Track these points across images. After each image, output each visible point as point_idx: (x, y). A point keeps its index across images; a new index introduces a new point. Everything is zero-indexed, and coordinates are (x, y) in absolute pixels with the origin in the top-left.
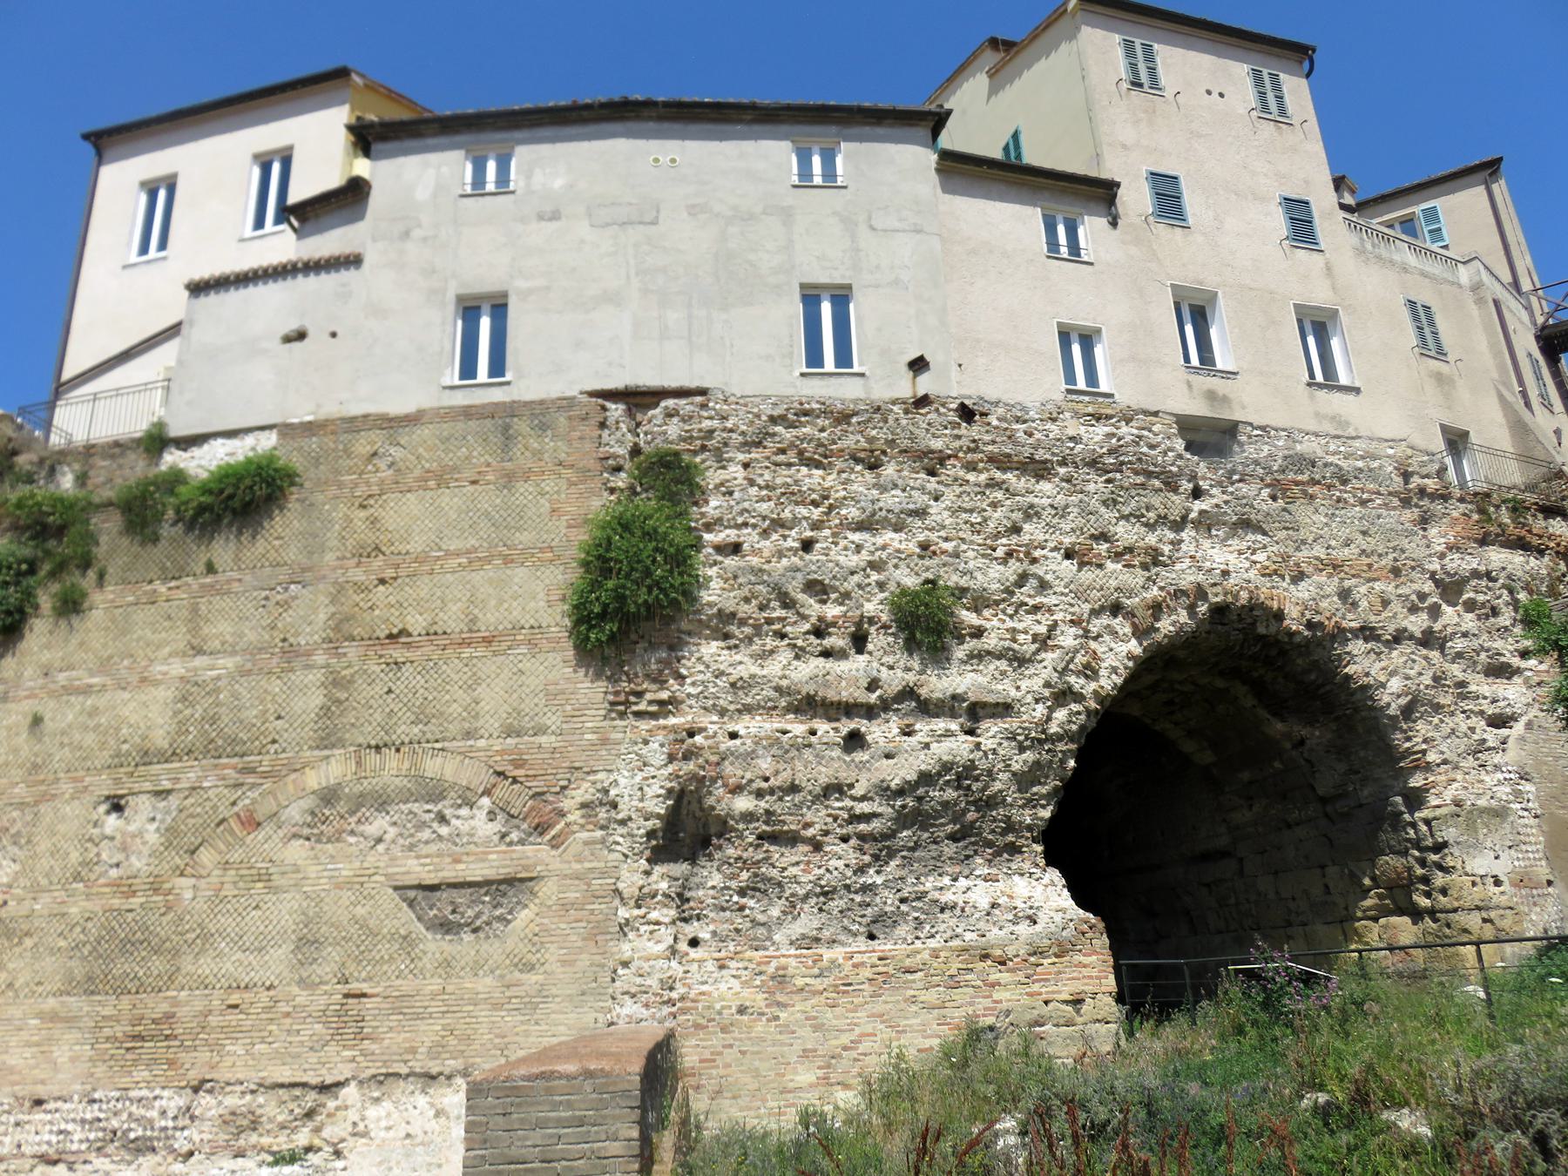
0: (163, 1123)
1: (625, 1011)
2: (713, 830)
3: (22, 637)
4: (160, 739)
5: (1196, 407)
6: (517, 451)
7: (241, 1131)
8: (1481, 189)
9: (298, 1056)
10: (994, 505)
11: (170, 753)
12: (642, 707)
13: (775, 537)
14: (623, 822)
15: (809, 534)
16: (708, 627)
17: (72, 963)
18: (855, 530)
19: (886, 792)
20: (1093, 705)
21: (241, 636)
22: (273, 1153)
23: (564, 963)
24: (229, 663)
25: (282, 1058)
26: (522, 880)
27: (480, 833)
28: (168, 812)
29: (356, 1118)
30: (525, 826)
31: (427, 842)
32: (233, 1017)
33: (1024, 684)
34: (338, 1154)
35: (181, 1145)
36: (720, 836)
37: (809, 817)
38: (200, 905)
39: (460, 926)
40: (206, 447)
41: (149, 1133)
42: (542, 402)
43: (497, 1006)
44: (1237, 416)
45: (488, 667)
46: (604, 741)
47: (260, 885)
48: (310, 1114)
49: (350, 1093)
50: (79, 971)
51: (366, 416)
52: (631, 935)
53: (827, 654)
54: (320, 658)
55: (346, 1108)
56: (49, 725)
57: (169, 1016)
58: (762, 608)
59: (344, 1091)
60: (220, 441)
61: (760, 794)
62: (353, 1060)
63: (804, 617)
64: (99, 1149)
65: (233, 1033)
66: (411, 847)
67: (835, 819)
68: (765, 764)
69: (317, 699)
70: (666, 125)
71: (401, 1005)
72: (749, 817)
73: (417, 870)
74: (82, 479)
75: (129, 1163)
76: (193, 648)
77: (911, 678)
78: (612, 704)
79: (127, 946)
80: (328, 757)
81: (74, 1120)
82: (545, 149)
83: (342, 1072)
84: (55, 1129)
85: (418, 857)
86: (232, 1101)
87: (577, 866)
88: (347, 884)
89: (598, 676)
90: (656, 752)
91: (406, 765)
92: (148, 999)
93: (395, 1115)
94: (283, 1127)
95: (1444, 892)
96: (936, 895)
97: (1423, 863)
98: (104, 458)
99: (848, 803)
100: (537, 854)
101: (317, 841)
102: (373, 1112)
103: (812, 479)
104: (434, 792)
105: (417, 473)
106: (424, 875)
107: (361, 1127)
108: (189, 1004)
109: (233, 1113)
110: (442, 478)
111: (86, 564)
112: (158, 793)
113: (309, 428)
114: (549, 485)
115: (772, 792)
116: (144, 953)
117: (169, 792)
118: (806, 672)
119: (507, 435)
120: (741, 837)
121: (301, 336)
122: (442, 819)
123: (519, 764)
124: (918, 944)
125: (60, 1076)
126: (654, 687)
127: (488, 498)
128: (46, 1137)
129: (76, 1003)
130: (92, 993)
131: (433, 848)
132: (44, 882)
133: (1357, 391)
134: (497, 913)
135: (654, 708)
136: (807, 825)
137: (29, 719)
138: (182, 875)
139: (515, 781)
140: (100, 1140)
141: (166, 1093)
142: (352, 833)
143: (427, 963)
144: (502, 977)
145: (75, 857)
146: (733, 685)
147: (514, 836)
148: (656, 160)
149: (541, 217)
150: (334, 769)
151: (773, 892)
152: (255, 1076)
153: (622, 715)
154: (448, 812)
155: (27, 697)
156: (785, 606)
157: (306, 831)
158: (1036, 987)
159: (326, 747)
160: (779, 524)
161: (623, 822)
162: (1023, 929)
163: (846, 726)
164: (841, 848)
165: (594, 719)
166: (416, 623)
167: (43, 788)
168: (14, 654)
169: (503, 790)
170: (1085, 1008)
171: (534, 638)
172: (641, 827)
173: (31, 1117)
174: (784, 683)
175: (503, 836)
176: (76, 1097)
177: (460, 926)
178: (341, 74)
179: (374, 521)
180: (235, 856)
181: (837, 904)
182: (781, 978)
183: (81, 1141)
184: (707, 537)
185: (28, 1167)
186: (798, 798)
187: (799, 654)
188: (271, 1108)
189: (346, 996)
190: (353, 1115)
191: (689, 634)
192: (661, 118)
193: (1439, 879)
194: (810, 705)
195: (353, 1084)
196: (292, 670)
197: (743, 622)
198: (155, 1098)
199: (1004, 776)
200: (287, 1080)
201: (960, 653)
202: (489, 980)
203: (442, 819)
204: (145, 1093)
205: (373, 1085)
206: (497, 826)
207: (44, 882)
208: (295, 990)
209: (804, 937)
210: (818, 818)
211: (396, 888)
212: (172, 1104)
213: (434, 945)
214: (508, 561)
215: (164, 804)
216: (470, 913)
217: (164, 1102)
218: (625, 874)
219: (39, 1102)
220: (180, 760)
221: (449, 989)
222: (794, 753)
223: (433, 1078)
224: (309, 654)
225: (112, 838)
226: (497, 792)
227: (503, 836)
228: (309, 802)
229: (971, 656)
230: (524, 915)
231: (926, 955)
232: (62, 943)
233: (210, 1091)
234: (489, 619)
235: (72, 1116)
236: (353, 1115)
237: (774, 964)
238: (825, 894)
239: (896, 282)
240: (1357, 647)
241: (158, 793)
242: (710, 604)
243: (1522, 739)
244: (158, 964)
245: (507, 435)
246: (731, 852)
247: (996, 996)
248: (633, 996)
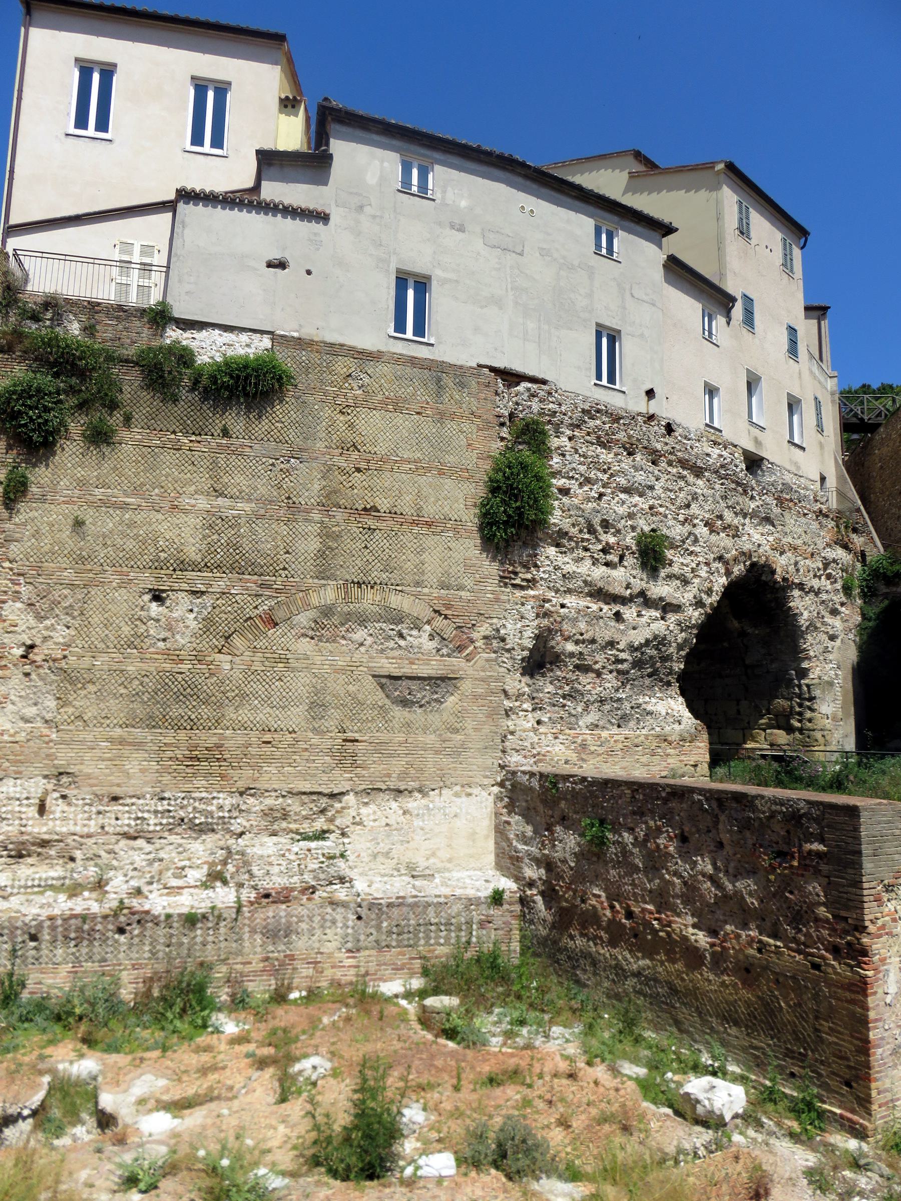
0: (221, 814)
1: (514, 759)
2: (547, 660)
3: (54, 454)
4: (192, 552)
5: (751, 447)
6: (446, 398)
7: (276, 819)
8: (815, 321)
9: (315, 775)
10: (681, 489)
11: (203, 564)
12: (518, 581)
13: (586, 488)
14: (508, 651)
15: (602, 490)
16: (551, 537)
17: (135, 705)
18: (622, 492)
19: (632, 648)
20: (709, 611)
21: (256, 489)
22: (301, 834)
23: (476, 730)
24: (248, 507)
25: (304, 776)
26: (450, 679)
27: (425, 647)
28: (204, 607)
29: (354, 814)
30: (451, 646)
31: (392, 649)
32: (267, 749)
33: (686, 595)
34: (343, 834)
35: (236, 828)
36: (551, 663)
37: (598, 658)
38: (237, 674)
39: (413, 703)
40: (204, 333)
41: (210, 820)
42: (461, 367)
43: (437, 752)
44: (764, 455)
45: (430, 541)
46: (497, 600)
47: (280, 665)
48: (323, 811)
49: (350, 799)
50: (140, 711)
51: (342, 345)
52: (513, 717)
53: (607, 564)
54: (316, 516)
55: (349, 808)
56: (90, 528)
57: (219, 746)
58: (581, 531)
59: (346, 798)
60: (217, 332)
61: (577, 642)
62: (351, 779)
63: (599, 541)
64: (170, 830)
65: (270, 759)
66: (382, 651)
67: (608, 660)
68: (582, 626)
69: (314, 545)
70: (528, 183)
71: (380, 748)
72: (572, 655)
73: (387, 666)
74: (89, 330)
75: (196, 839)
76: (216, 491)
77: (644, 585)
78: (501, 577)
79: (181, 697)
80: (324, 585)
81: (149, 811)
82: (454, 174)
83: (345, 786)
84: (133, 816)
85: (387, 658)
86: (270, 802)
87: (482, 674)
88: (342, 671)
89: (494, 559)
90: (529, 610)
91: (378, 598)
92: (203, 734)
93: (379, 813)
94: (306, 818)
95: (810, 720)
96: (644, 706)
97: (800, 705)
98: (107, 315)
99: (614, 652)
100: (457, 663)
101: (319, 640)
102: (364, 811)
103: (606, 456)
104: (397, 618)
105: (380, 397)
106: (392, 670)
107: (358, 819)
108: (233, 740)
109: (272, 809)
110: (397, 405)
111: (113, 406)
112: (194, 593)
113: (300, 343)
114: (466, 426)
115: (583, 642)
116: (194, 703)
117: (203, 593)
118: (599, 573)
119: (440, 388)
120: (566, 666)
121: (281, 265)
122: (401, 636)
123: (448, 607)
124: (638, 732)
125: (132, 781)
126: (523, 570)
127: (429, 428)
128: (127, 822)
129: (138, 733)
130: (154, 727)
131: (396, 653)
132: (101, 646)
133: (803, 449)
134: (435, 696)
135: (525, 584)
136: (596, 662)
137: (70, 521)
138: (220, 652)
139: (446, 617)
140: (170, 824)
141: (221, 795)
142: (343, 637)
143: (396, 724)
144: (440, 735)
145: (126, 630)
146: (564, 576)
147: (445, 651)
148: (523, 207)
149: (452, 227)
150: (329, 595)
151: (579, 698)
152: (286, 787)
153: (506, 584)
154: (404, 631)
155: (65, 502)
156: (589, 532)
157: (311, 633)
158: (682, 758)
159: (323, 578)
160: (588, 481)
161: (508, 651)
162: (676, 726)
163: (617, 608)
164: (609, 677)
165: (492, 584)
166: (383, 504)
167: (91, 575)
168: (47, 466)
169: (439, 622)
170: (698, 769)
171: (457, 527)
172: (519, 655)
173: (107, 809)
174: (589, 579)
175: (438, 650)
176: (148, 796)
177: (413, 703)
178: (280, 38)
179: (351, 426)
180: (261, 643)
181: (607, 707)
182: (584, 746)
183: (156, 825)
184: (554, 481)
185: (113, 841)
186: (594, 646)
187: (595, 562)
188: (293, 805)
189: (344, 740)
190: (353, 812)
191: (541, 540)
192: (526, 177)
193: (808, 714)
194: (600, 594)
195: (352, 794)
196: (296, 520)
197: (571, 539)
198: (214, 798)
199: (674, 645)
200: (308, 790)
201: (663, 573)
202: (433, 737)
203: (401, 636)
204: (204, 795)
205: (364, 795)
206: (433, 645)
207: (101, 646)
208: (310, 735)
209: (592, 724)
210: (600, 658)
211: (374, 676)
212: (227, 802)
213: (399, 713)
214: (441, 473)
215: (200, 600)
216: (419, 695)
217: (221, 801)
218: (508, 679)
219: (115, 799)
220: (212, 571)
221: (410, 740)
222: (595, 621)
223: (400, 792)
224: (308, 512)
225: (158, 621)
226: (434, 623)
227: (438, 650)
228: (312, 614)
229: (668, 576)
230: (451, 700)
231: (642, 738)
232: (123, 691)
233: (252, 795)
234: (430, 510)
235: (147, 808)
236: (353, 812)
237: (581, 738)
238: (601, 701)
239: (642, 336)
240: (796, 593)
241: (194, 593)
242: (554, 524)
243: (839, 648)
244: (205, 711)
245: (440, 388)
246: (559, 673)
247: (669, 761)
248: (518, 751)
